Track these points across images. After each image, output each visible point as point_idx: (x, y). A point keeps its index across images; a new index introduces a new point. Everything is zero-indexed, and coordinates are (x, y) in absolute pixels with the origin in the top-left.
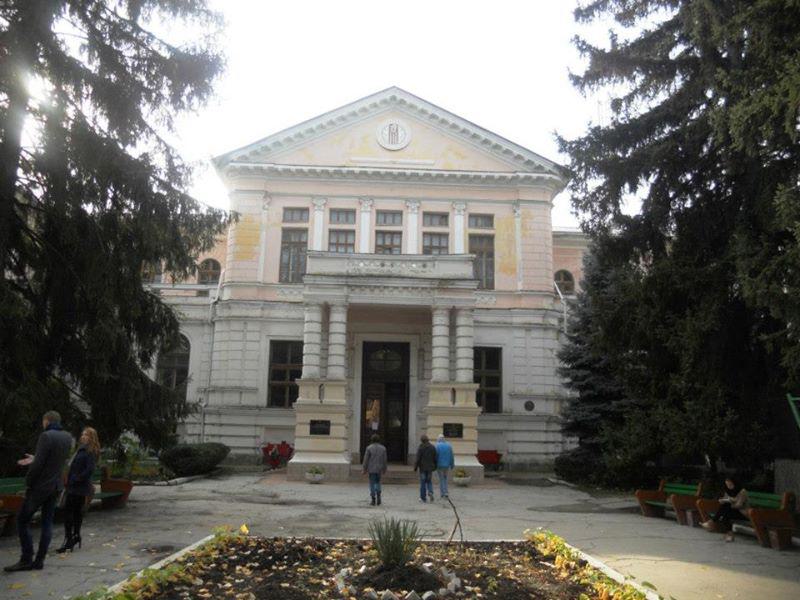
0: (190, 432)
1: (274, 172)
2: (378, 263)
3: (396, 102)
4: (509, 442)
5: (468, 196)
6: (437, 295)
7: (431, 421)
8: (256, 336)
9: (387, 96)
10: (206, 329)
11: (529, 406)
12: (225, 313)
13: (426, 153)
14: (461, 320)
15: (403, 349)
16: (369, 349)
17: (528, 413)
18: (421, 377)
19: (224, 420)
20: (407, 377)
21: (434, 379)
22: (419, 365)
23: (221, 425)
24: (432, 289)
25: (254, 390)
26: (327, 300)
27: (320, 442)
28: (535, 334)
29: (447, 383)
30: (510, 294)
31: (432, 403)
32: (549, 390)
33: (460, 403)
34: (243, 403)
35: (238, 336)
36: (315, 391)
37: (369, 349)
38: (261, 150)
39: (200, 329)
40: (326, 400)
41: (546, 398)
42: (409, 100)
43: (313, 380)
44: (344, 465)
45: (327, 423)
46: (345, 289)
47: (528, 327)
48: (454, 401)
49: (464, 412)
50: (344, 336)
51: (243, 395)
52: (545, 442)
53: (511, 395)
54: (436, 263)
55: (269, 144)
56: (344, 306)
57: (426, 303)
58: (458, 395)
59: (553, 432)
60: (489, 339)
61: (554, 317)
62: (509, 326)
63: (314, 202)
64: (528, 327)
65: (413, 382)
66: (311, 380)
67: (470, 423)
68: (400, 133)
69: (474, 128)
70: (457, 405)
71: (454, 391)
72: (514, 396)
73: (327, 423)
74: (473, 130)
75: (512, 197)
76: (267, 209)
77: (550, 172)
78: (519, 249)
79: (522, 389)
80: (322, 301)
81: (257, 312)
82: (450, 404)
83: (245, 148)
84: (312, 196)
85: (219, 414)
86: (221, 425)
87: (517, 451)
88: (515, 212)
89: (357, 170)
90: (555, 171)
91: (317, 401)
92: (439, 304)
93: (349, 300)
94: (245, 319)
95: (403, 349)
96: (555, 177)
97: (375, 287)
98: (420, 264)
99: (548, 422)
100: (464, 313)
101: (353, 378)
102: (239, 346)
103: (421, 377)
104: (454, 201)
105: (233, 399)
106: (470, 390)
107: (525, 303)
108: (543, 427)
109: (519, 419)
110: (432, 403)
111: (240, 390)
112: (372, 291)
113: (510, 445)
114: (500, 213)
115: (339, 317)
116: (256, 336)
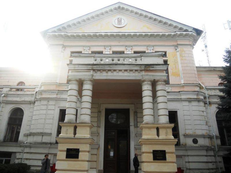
0: (17, 157)
1: (68, 37)
2: (110, 59)
3: (120, 9)
4: (186, 162)
5: (154, 44)
6: (143, 73)
7: (145, 148)
8: (53, 107)
9: (117, 6)
10: (32, 106)
11: (195, 141)
12: (40, 96)
13: (132, 26)
14: (159, 87)
15: (126, 113)
16: (108, 112)
17: (195, 145)
18: (136, 126)
19: (32, 150)
20: (128, 126)
21: (145, 121)
22: (134, 120)
23: (31, 153)
24: (141, 70)
25: (50, 134)
26: (80, 77)
27: (72, 164)
28: (194, 103)
29: (153, 124)
30: (179, 85)
31: (144, 137)
32: (204, 132)
33: (162, 136)
34: (44, 141)
35: (44, 107)
36: (72, 130)
37: (108, 112)
38: (62, 28)
39: (29, 106)
40: (77, 136)
41: (203, 136)
42: (126, 7)
43: (70, 123)
44: (218, 111)
45: (77, 151)
46: (92, 71)
47: (190, 100)
48: (158, 135)
49: (165, 142)
50: (90, 104)
51: (43, 137)
52: (207, 162)
53: (184, 135)
54: (142, 57)
55: (65, 26)
56: (91, 80)
57: (138, 78)
58: (161, 131)
59: (210, 156)
60: (173, 106)
61: (202, 95)
62: (181, 100)
63: (85, 48)
64: (190, 100)
65: (132, 129)
66: (69, 123)
67: (170, 149)
68: (123, 21)
69: (155, 16)
70: (161, 137)
71: (158, 129)
72: (186, 136)
73: (77, 151)
74: (154, 17)
75: (175, 44)
76: (63, 52)
77: (191, 31)
78: (180, 66)
79: (189, 132)
80: (78, 78)
81: (54, 96)
82: (157, 137)
83: (55, 27)
84: (84, 46)
85: (30, 147)
86: (31, 153)
87: (191, 167)
88: (176, 50)
89: (103, 34)
90: (194, 31)
91: (72, 135)
92: (146, 78)
93: (93, 78)
94: (48, 99)
95: (126, 113)
96: (194, 34)
97: (109, 70)
98: (134, 59)
99: (207, 150)
100: (160, 83)
101: (100, 127)
102: (44, 112)
103: (136, 126)
104: (148, 46)
105: (38, 139)
106: (168, 128)
107: (186, 89)
108: (204, 153)
109: (191, 149)
110: (144, 137)
111: (42, 134)
112: (107, 72)
113: (187, 164)
114: (170, 51)
115: (88, 87)
116: (53, 107)
